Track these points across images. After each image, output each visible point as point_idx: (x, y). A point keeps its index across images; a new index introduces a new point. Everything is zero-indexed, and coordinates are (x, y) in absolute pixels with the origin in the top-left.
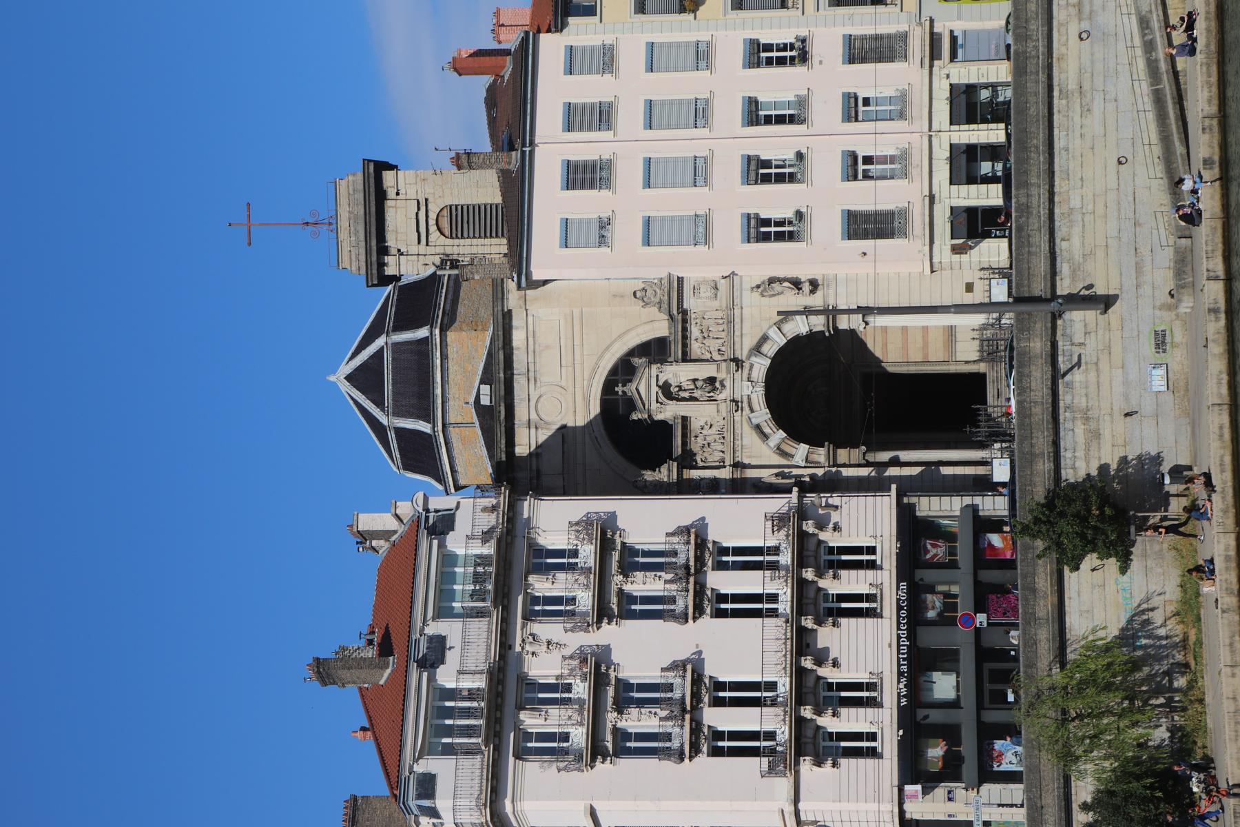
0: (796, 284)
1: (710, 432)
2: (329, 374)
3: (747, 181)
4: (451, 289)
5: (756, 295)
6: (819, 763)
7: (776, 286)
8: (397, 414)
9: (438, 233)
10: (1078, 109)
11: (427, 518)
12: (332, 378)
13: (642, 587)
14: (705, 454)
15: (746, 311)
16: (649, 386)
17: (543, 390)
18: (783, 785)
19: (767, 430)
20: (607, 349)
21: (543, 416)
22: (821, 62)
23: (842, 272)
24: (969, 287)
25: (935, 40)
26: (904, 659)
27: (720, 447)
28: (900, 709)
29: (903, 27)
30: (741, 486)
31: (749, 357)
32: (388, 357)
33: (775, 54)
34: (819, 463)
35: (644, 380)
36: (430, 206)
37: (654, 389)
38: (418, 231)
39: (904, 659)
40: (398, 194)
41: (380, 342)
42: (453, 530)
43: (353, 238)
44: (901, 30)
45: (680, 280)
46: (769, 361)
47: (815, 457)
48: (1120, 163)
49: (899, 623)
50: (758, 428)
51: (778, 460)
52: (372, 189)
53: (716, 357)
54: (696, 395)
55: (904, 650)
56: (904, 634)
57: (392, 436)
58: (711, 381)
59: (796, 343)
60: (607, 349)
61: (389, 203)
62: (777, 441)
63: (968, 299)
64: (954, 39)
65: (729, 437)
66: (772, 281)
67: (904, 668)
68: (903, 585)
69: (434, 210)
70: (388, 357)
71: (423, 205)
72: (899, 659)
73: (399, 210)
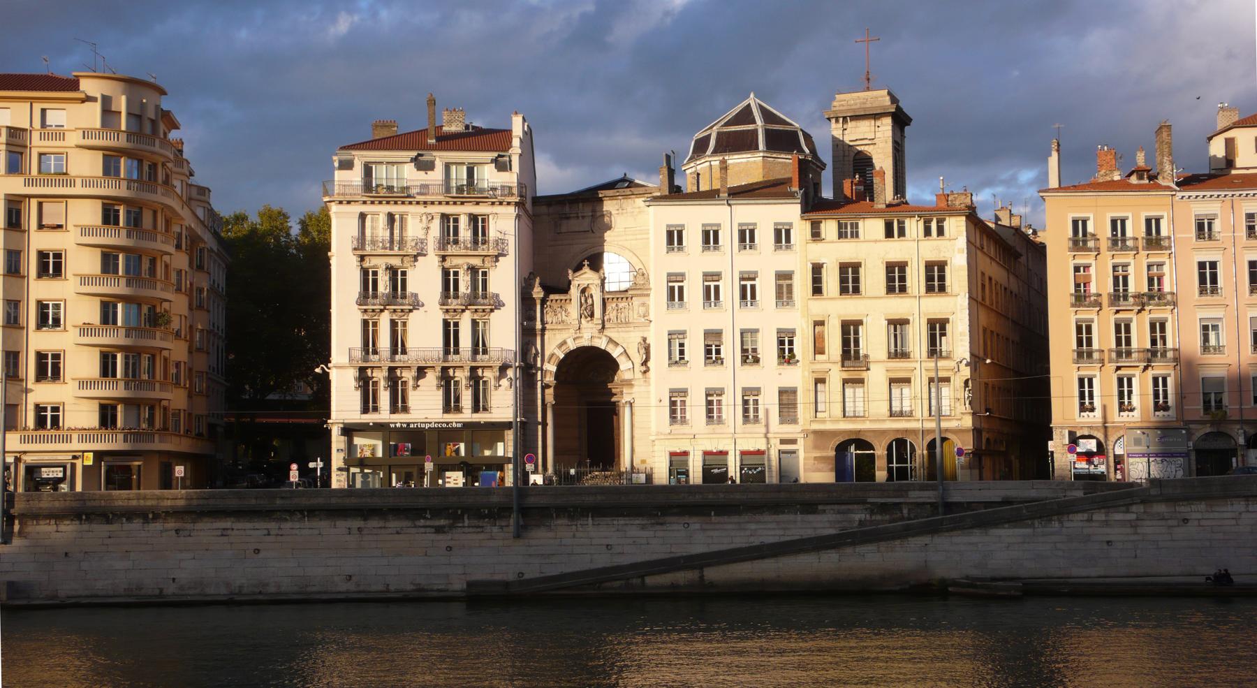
0: (645, 363)
2: (754, 93)
3: (779, 331)
5: (640, 340)
7: (643, 351)
8: (719, 134)
10: (643, 522)
12: (752, 96)
14: (550, 313)
16: (588, 279)
19: (564, 348)
22: (780, 374)
23: (652, 388)
25: (794, 442)
26: (417, 426)
27: (554, 321)
28: (388, 424)
29: (801, 421)
31: (606, 336)
32: (751, 127)
33: (787, 347)
34: (545, 378)
35: (591, 276)
36: (872, 146)
37: (586, 283)
38: (857, 140)
39: (417, 426)
40: (878, 127)
41: (759, 122)
42: (418, 170)
43: (852, 102)
44: (799, 421)
45: (648, 295)
46: (603, 348)
48: (608, 545)
49: (438, 423)
50: (564, 343)
54: (584, 306)
55: (423, 426)
58: (592, 315)
61: (873, 122)
62: (557, 354)
64: (794, 452)
65: (559, 327)
66: (647, 350)
67: (412, 426)
68: (459, 425)
70: (751, 127)
72: (418, 423)
73: (869, 128)
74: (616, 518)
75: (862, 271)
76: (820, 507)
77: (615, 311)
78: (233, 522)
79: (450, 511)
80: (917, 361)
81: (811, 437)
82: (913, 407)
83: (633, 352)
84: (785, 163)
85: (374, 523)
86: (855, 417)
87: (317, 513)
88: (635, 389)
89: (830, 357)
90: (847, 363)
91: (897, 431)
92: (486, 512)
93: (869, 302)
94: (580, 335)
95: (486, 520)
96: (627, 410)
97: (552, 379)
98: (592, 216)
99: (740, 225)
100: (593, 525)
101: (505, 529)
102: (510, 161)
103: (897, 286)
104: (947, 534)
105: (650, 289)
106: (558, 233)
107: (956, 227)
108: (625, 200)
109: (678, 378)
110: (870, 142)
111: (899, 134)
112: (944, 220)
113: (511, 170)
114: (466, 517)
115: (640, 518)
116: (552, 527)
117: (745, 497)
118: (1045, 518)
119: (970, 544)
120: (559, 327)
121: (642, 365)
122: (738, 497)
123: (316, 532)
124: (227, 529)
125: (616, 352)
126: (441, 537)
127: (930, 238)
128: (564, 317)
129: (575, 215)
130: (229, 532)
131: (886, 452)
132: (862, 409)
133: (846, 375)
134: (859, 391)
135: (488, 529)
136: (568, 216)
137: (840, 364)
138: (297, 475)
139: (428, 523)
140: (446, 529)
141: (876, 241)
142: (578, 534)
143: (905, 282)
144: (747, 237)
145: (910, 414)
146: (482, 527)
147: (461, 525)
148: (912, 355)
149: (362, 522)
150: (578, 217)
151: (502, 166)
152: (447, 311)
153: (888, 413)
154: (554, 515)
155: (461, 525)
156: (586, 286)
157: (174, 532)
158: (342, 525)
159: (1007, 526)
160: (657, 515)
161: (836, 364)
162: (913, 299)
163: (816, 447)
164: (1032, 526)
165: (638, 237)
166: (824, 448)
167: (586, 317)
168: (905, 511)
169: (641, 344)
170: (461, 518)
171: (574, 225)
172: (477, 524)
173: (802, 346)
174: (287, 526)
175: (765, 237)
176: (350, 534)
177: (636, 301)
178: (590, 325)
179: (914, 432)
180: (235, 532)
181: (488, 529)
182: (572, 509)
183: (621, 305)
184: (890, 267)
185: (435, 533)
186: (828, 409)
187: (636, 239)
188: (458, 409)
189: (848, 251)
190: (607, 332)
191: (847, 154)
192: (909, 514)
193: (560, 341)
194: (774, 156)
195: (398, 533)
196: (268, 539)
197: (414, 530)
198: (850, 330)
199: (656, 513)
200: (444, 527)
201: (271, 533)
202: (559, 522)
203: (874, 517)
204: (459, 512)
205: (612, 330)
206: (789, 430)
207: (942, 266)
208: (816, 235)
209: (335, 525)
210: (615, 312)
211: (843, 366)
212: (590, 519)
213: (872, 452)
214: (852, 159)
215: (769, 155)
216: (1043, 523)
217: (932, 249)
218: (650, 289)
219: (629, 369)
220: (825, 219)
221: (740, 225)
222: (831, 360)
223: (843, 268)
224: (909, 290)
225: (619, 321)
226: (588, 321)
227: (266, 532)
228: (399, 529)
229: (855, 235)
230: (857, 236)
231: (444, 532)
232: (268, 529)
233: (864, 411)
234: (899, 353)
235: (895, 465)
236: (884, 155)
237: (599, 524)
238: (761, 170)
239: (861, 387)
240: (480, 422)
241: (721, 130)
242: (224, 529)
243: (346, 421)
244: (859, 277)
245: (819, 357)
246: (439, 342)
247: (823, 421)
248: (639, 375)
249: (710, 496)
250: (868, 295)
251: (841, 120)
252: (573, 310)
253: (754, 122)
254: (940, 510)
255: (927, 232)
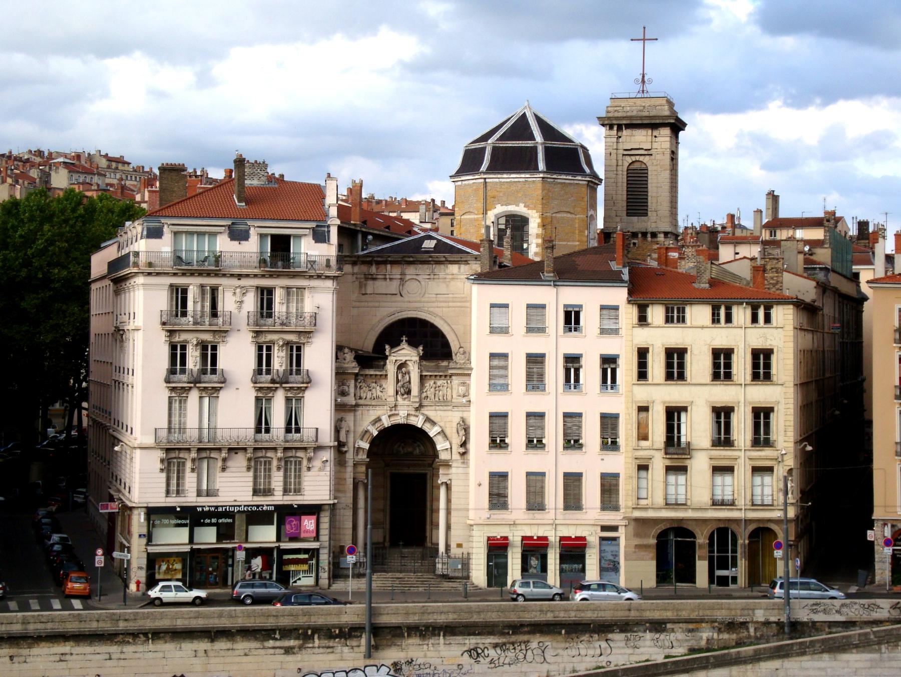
0: (464, 444)
1: (378, 391)
4: (572, 182)
6: (162, 461)
7: (462, 432)
8: (495, 150)
9: (630, 161)
11: (324, 226)
13: (276, 355)
15: (450, 413)
16: (405, 355)
17: (423, 283)
18: (150, 440)
19: (378, 425)
20: (446, 322)
21: (408, 283)
22: (602, 460)
24: (459, 546)
25: (615, 528)
26: (226, 509)
27: (369, 397)
30: (341, 408)
31: (423, 414)
32: (529, 144)
35: (409, 352)
36: (648, 157)
37: (404, 359)
38: (632, 149)
39: (226, 509)
40: (655, 137)
41: (539, 138)
42: (316, 242)
43: (628, 108)
45: (469, 375)
46: (420, 426)
47: (361, 453)
48: (459, 665)
49: (248, 506)
50: (378, 420)
51: (360, 430)
52: (658, 121)
53: (424, 395)
55: (232, 509)
56: (242, 509)
57: (482, 145)
58: (409, 392)
59: (430, 442)
60: (446, 322)
61: (650, 131)
62: (371, 430)
63: (453, 545)
64: (615, 539)
65: (373, 403)
66: (466, 430)
67: (220, 509)
69: (645, 159)
70: (529, 144)
71: (648, 153)
74: (468, 637)
75: (688, 357)
76: (669, 626)
77: (433, 389)
78: (72, 647)
79: (300, 631)
80: (741, 450)
81: (633, 523)
82: (736, 496)
83: (451, 431)
84: (564, 183)
85: (222, 645)
86: (677, 504)
87: (162, 635)
88: (453, 470)
89: (654, 443)
90: (671, 450)
91: (719, 520)
92: (337, 632)
93: (693, 388)
94: (396, 412)
95: (337, 640)
96: (443, 491)
97: (365, 457)
98: (401, 279)
99: (565, 306)
100: (445, 644)
101: (356, 649)
102: (329, 232)
103: (722, 373)
104: (797, 659)
105: (471, 369)
106: (363, 294)
107: (784, 315)
108: (437, 266)
109: (499, 462)
110: (646, 153)
111: (674, 142)
112: (772, 307)
113: (329, 241)
114: (316, 636)
115: (492, 637)
116: (403, 646)
117: (595, 615)
118: (892, 644)
119: (819, 669)
120: (373, 403)
121: (461, 446)
122: (589, 615)
123: (161, 655)
124: (66, 654)
125: (433, 431)
126: (290, 658)
127: (757, 325)
128: (379, 393)
129: (383, 277)
130: (68, 657)
131: (708, 541)
132: (684, 497)
133: (668, 463)
134: (682, 479)
135: (339, 649)
136: (374, 276)
137: (663, 451)
138: (103, 560)
139: (278, 644)
140: (296, 650)
141: (703, 327)
142: (429, 654)
143: (730, 369)
144: (572, 318)
145: (733, 504)
146: (332, 647)
147: (311, 645)
148: (736, 443)
149: (209, 644)
150: (385, 279)
151: (320, 236)
152: (260, 389)
153: (710, 502)
154: (406, 634)
155: (311, 645)
156: (403, 362)
157: (8, 658)
158: (188, 647)
159: (854, 651)
160: (508, 633)
161: (659, 451)
162: (739, 387)
163: (637, 535)
164: (879, 651)
165: (451, 304)
166: (646, 536)
167: (403, 395)
168: (752, 630)
169: (461, 426)
170: (311, 638)
171: (380, 286)
172: (327, 645)
173: (626, 432)
174: (129, 649)
175: (590, 319)
176: (196, 656)
177: (456, 381)
178: (406, 402)
179: (737, 521)
180: (74, 657)
181: (339, 649)
182: (423, 629)
183: (439, 383)
184: (716, 353)
185: (284, 654)
186: (650, 496)
187: (449, 307)
188: (268, 492)
189: (674, 336)
190: (425, 411)
191: (620, 163)
192: (755, 633)
193: (373, 418)
194: (555, 176)
195: (246, 655)
196: (109, 663)
197: (262, 652)
198: (673, 414)
199: (506, 631)
200: (292, 648)
201: (113, 657)
202: (411, 641)
203: (721, 636)
204: (310, 632)
205: (429, 408)
206: (610, 518)
207: (768, 353)
208: (643, 320)
209: (181, 648)
210: (433, 390)
211: (666, 454)
212: (441, 637)
213: (692, 539)
214: (625, 169)
215: (549, 176)
216: (890, 648)
217: (760, 337)
218: (471, 369)
219: (447, 449)
220: (652, 304)
221: (565, 306)
222: (655, 447)
223: (670, 353)
224: (735, 378)
225: (437, 399)
226: (405, 399)
227: (107, 656)
228: (247, 651)
229: (682, 319)
230: (684, 321)
231: (294, 653)
232: (109, 653)
233: (686, 499)
234: (723, 438)
235: (716, 554)
236: (661, 168)
237: (450, 644)
238: (540, 192)
239: (684, 474)
240: (291, 505)
241: (497, 145)
242: (62, 654)
243: (150, 505)
244: (684, 363)
245: (644, 444)
246: (251, 423)
247: (645, 509)
248: (456, 456)
249: (562, 614)
250: (694, 381)
251: (615, 128)
252: (390, 386)
253: (532, 138)
254: (786, 629)
255: (755, 319)
